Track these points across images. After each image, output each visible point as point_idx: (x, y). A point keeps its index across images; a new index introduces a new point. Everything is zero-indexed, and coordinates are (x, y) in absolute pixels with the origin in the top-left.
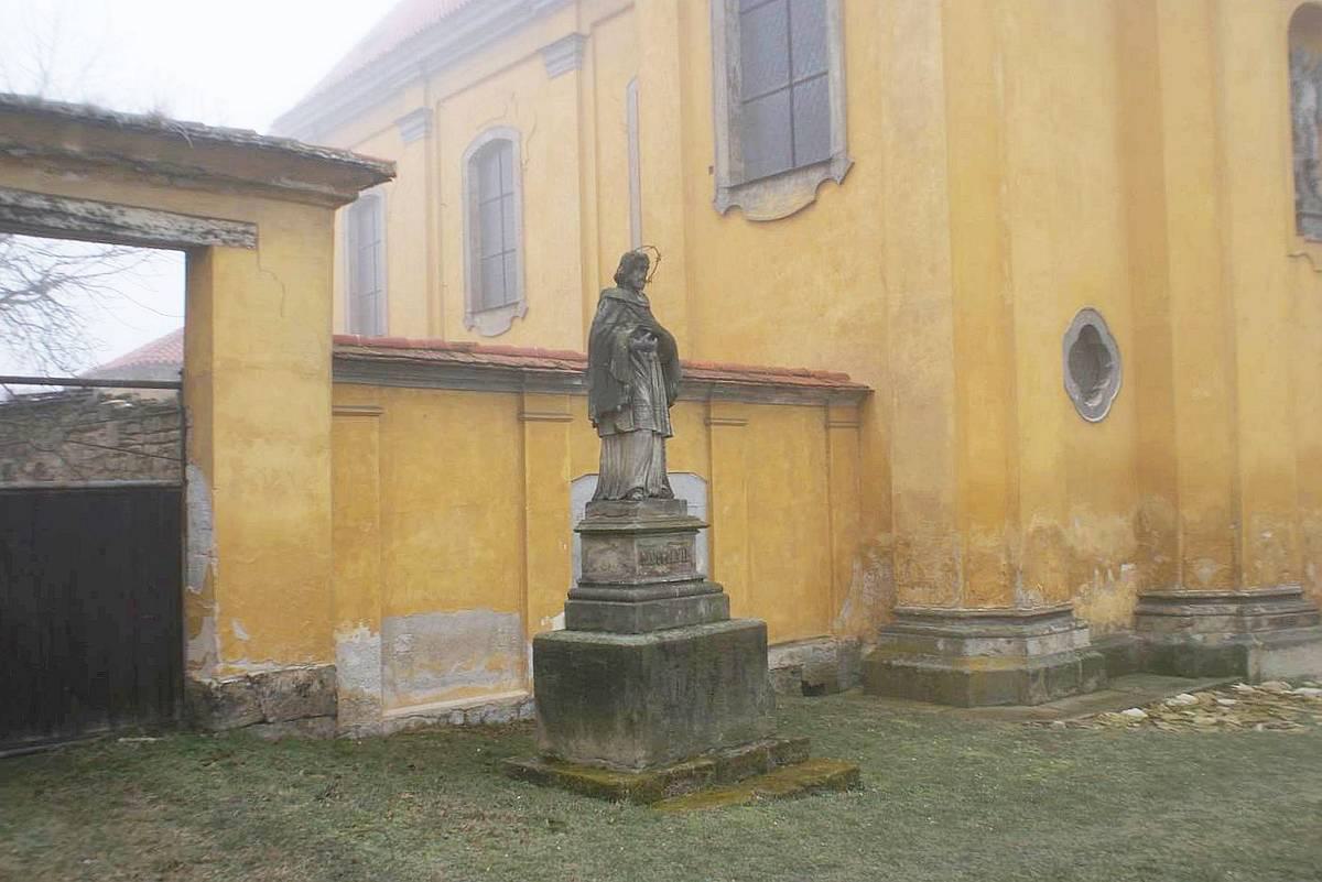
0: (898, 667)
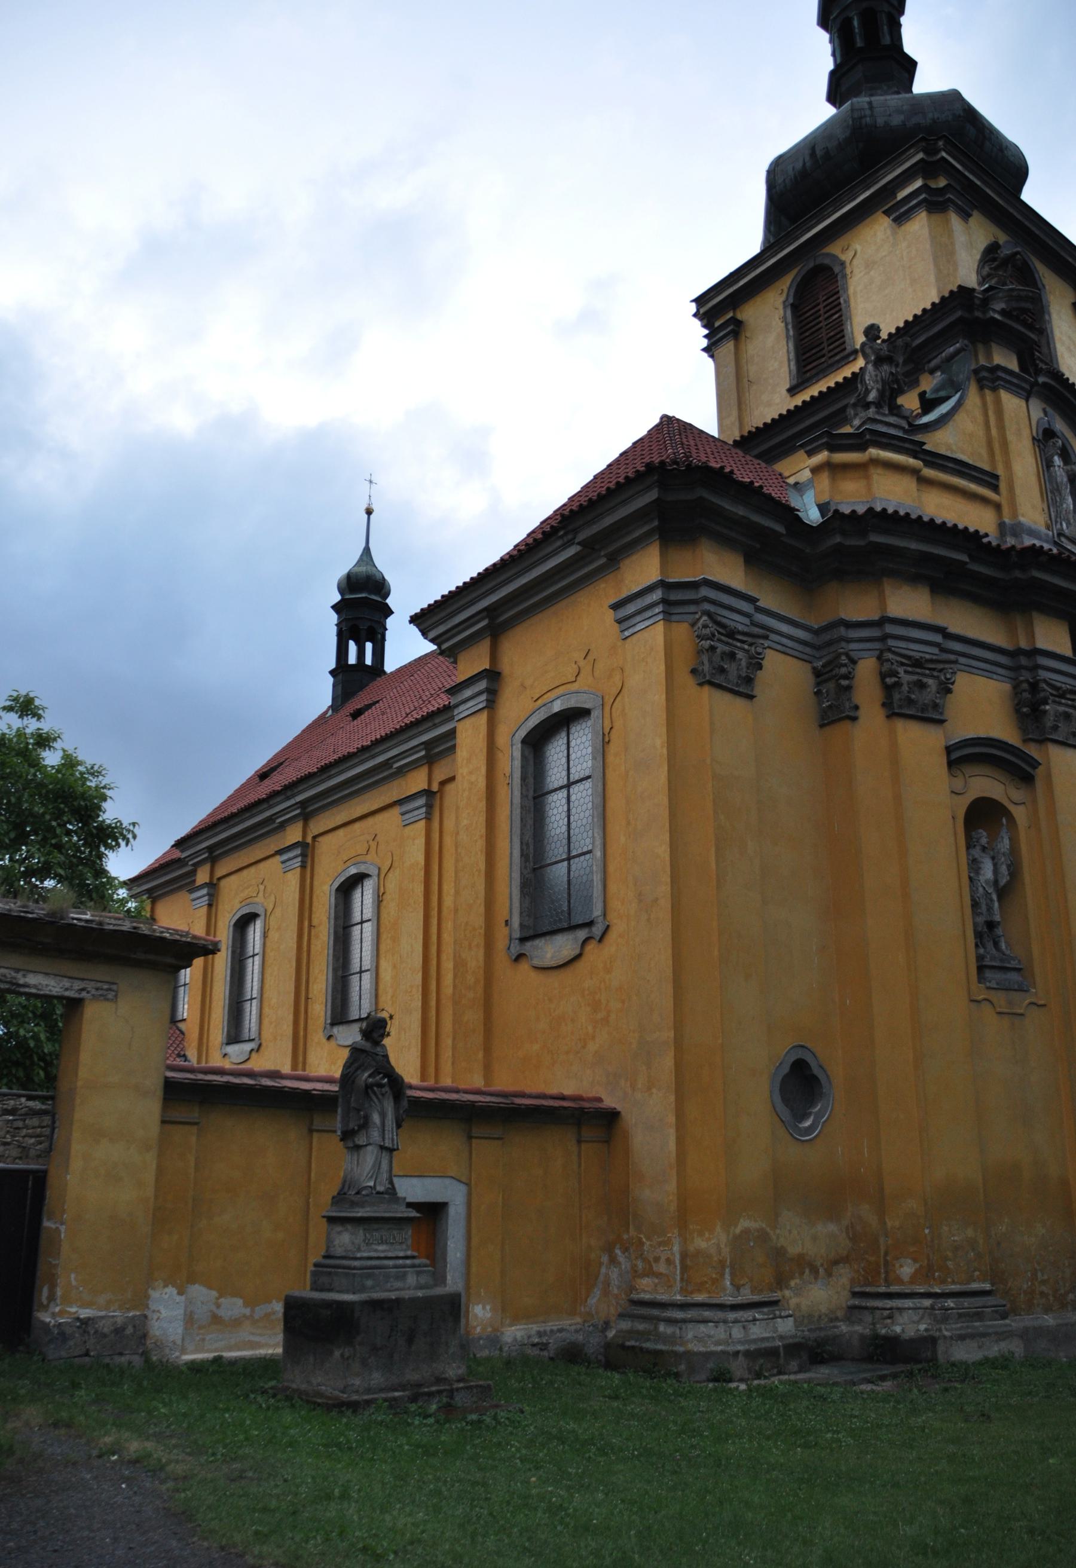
0: (629, 1347)
